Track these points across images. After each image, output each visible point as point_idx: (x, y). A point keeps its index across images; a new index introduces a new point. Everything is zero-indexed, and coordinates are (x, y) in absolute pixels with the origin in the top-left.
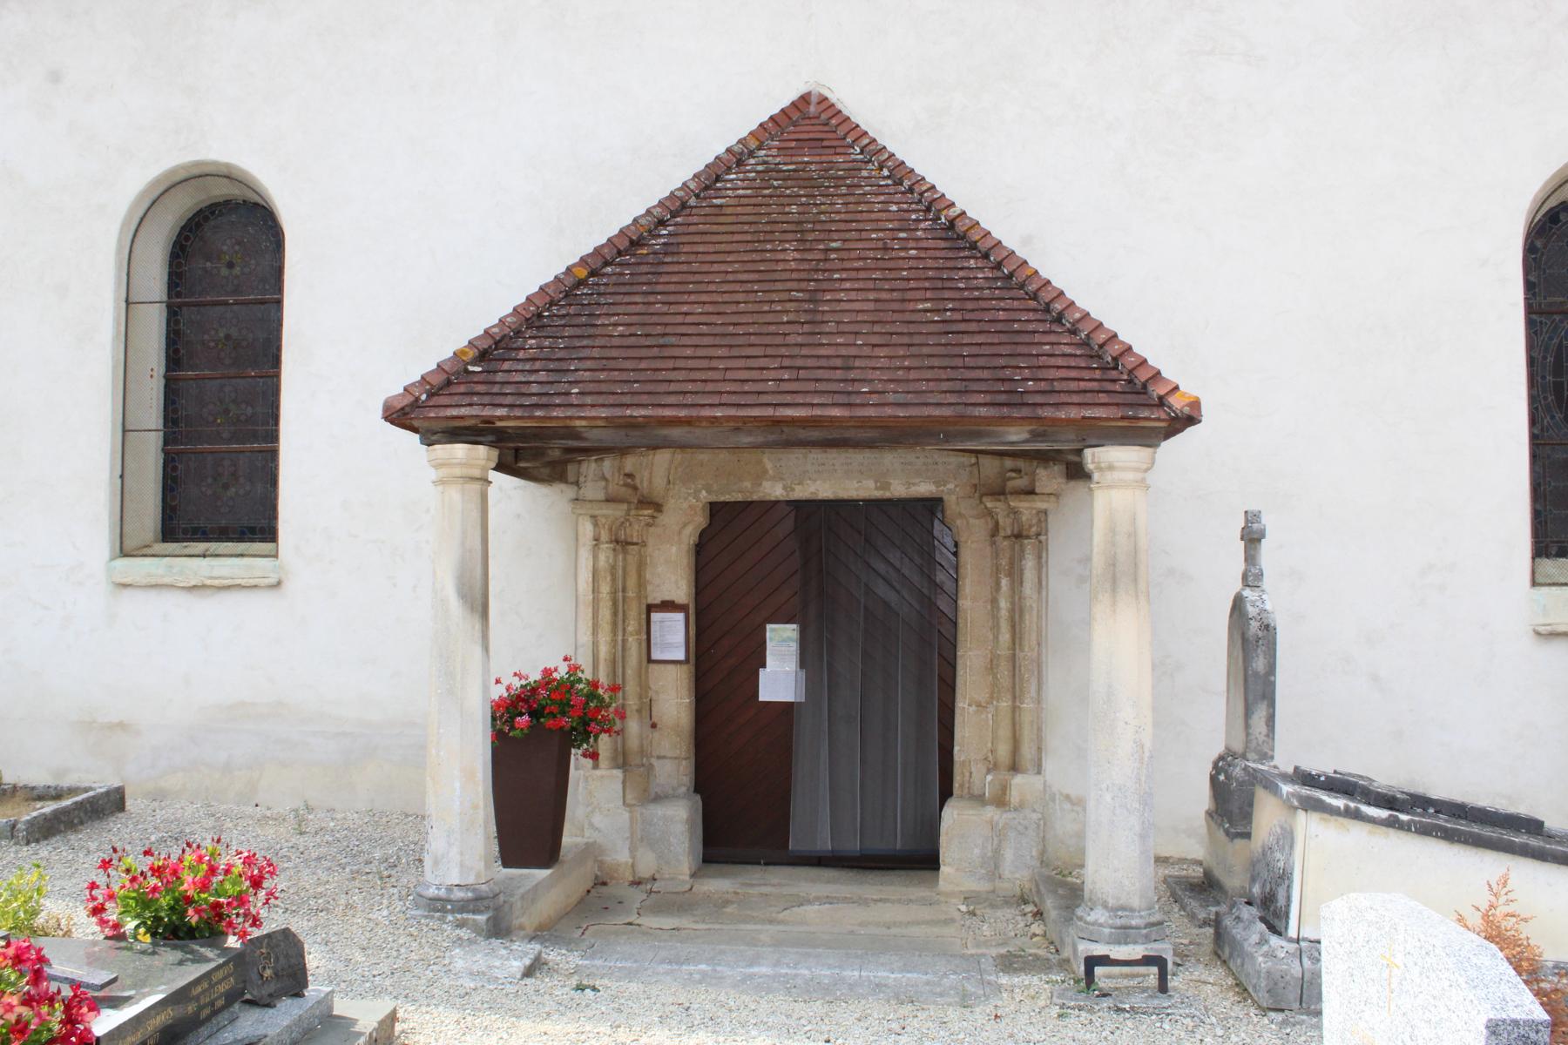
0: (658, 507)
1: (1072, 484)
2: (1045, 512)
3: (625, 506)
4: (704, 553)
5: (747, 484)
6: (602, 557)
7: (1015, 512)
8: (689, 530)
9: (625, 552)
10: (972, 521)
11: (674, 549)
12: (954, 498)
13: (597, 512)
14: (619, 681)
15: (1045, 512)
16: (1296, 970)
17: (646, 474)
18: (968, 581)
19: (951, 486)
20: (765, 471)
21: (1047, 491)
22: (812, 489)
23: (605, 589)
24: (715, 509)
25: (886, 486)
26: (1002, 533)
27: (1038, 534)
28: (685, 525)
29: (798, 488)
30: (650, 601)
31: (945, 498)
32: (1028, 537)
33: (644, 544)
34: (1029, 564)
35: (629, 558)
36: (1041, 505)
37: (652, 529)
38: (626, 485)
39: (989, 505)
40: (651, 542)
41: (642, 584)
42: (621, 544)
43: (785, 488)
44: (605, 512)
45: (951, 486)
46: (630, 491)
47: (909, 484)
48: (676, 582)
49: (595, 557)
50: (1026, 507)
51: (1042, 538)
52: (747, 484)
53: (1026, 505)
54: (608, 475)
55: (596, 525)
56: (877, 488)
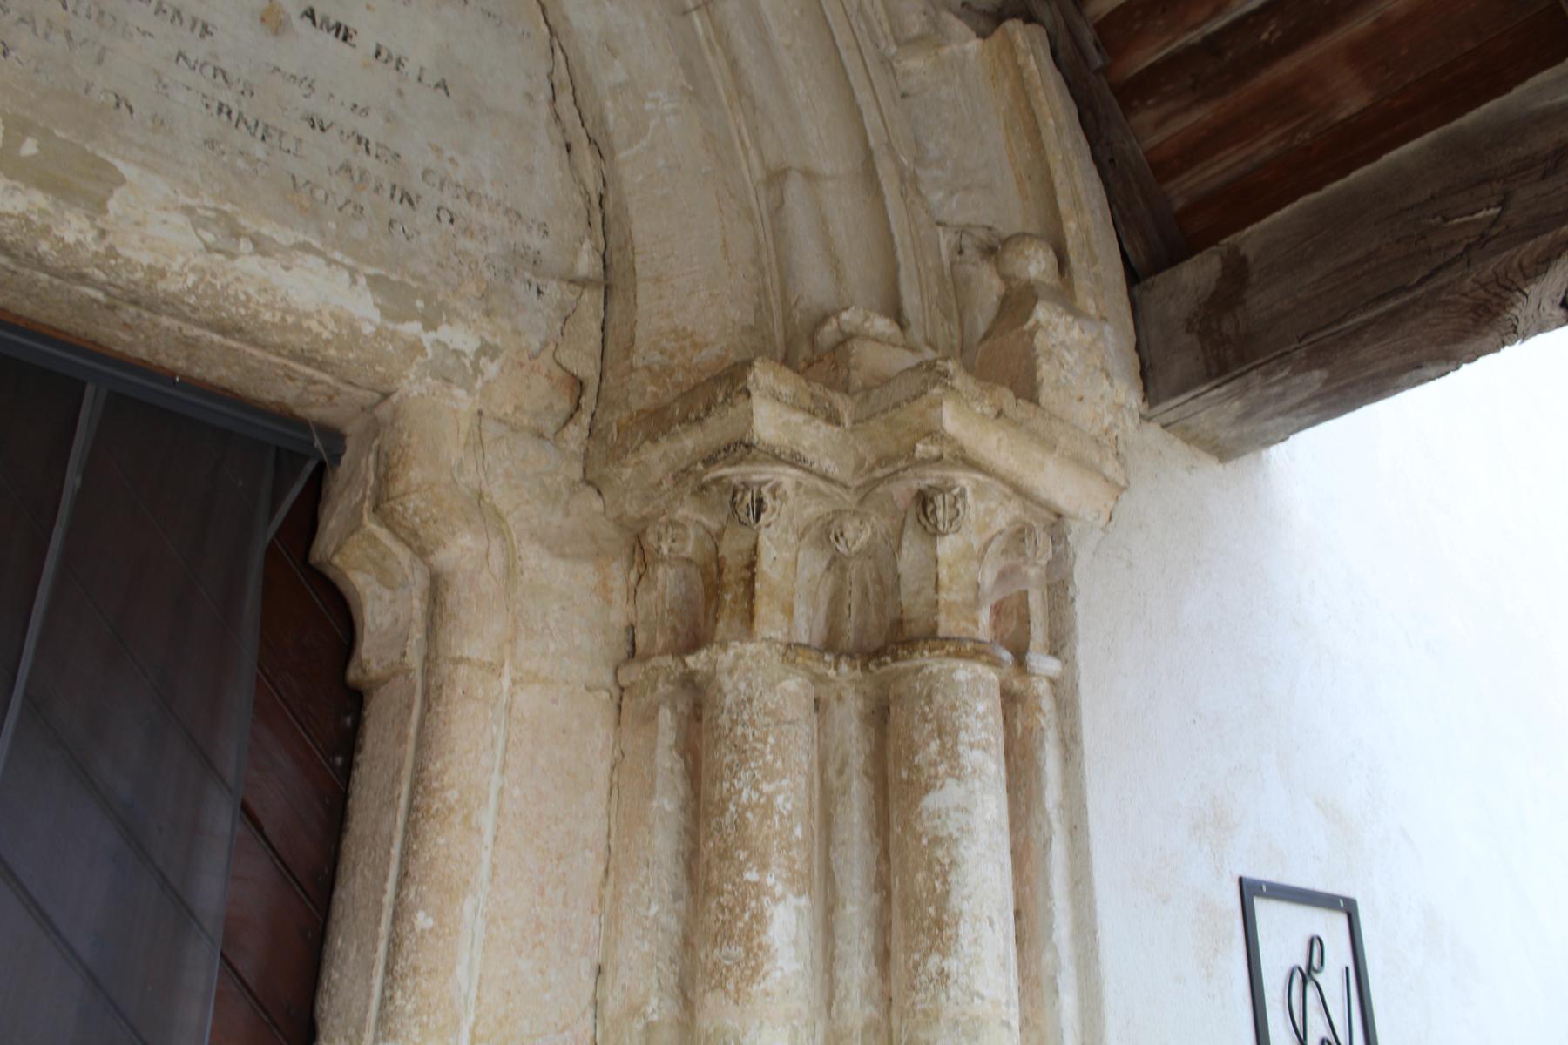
10: (533, 557)
12: (463, 401)
18: (471, 911)
19: (461, 337)
26: (770, 622)
31: (413, 385)
34: (971, 806)
45: (461, 337)
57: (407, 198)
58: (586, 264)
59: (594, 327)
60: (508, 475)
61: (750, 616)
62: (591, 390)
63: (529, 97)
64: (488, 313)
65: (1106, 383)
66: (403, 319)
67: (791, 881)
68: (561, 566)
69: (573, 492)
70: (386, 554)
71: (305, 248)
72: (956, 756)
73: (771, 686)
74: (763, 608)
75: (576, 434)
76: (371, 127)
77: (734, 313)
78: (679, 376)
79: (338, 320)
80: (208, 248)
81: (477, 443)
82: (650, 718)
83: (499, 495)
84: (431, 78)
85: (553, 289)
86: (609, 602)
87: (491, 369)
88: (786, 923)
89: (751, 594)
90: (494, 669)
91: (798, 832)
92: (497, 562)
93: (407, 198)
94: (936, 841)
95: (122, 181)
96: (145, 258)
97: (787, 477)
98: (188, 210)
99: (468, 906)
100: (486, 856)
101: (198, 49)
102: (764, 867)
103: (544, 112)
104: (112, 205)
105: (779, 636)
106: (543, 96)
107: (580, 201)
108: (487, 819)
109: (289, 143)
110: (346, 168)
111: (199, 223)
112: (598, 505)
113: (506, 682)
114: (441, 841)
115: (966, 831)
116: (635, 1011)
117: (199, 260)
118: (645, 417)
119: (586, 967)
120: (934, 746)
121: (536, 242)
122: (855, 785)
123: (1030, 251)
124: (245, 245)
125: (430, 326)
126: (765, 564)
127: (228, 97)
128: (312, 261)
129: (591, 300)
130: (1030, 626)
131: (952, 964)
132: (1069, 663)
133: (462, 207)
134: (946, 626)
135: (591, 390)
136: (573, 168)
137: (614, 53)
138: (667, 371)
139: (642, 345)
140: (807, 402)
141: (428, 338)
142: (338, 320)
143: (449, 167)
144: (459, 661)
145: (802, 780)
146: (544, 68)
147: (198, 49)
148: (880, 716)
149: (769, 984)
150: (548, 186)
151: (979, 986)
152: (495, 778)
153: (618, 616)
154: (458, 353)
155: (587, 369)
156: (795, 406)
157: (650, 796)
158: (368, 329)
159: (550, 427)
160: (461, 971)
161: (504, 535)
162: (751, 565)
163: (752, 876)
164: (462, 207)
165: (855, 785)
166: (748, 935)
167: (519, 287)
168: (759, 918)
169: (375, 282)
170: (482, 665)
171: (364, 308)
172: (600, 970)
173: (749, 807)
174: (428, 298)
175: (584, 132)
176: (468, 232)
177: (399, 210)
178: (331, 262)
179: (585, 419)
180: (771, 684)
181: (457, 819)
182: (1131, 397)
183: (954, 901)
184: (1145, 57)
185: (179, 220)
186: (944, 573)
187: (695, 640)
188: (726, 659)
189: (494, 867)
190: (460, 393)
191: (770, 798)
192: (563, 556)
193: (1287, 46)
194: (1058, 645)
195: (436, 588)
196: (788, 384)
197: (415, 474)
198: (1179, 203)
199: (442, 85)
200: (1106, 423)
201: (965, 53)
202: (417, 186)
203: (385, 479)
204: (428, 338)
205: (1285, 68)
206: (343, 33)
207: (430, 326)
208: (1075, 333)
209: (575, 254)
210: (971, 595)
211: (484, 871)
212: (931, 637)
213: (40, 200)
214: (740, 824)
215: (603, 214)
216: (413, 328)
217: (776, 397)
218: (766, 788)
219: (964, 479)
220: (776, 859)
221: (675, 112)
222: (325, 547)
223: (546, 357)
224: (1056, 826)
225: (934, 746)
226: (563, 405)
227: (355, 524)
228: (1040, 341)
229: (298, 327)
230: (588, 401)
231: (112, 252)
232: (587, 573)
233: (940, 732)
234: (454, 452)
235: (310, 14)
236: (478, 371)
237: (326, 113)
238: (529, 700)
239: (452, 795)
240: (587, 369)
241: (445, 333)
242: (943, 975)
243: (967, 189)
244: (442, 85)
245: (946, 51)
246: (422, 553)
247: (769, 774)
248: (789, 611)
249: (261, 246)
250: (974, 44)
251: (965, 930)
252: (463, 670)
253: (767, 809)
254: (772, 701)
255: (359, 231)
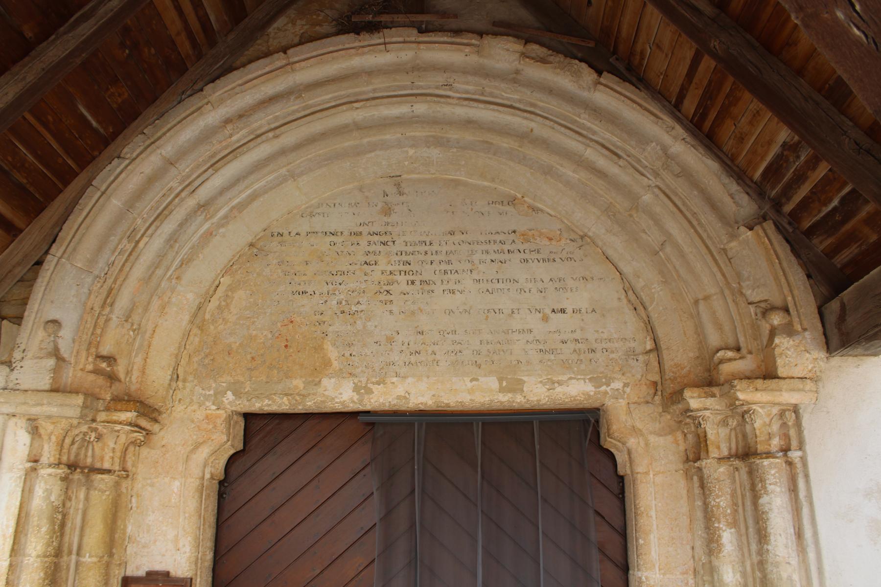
0: (148, 411)
1: (836, 360)
2: (796, 410)
3: (79, 400)
4: (229, 492)
5: (298, 383)
6: (39, 491)
7: (744, 415)
8: (204, 452)
9: (89, 486)
10: (652, 439)
11: (177, 483)
12: (623, 402)
13: (35, 410)
14: (737, 473)
15: (796, 410)
16: (75, 300)
17: (138, 360)
18: (653, 538)
19: (617, 385)
20: (327, 363)
21: (798, 372)
22: (400, 391)
23: (36, 546)
24: (255, 424)
25: (516, 386)
26: (714, 453)
27: (786, 450)
28: (197, 446)
29: (377, 389)
30: (131, 571)
31: (609, 402)
32: (769, 455)
33: (126, 473)
34: (776, 502)
35: (94, 494)
36: (789, 398)
37: (145, 451)
38: (96, 371)
39: (694, 404)
40: (141, 471)
41: (113, 540)
42: (76, 469)
43: (356, 389)
44: (54, 410)
45: (617, 385)
46: (101, 381)
47: (552, 383)
48: (176, 539)
49: (27, 492)
50: (762, 401)
51: (795, 455)
52: (298, 383)
53: (759, 396)
54: (65, 352)
55: (35, 431)
56: (502, 390)
57: (593, 351)
58: (649, 345)
59: (656, 364)
60: (640, 418)
61: (707, 452)
62: (659, 383)
63: (619, 299)
64: (623, 374)
65: (807, 355)
66: (600, 387)
67: (728, 525)
68: (661, 439)
69: (661, 416)
70: (615, 445)
71: (571, 378)
72: (766, 488)
73: (715, 471)
74: (710, 449)
75: (657, 398)
76: (577, 335)
77: (691, 355)
78: (679, 380)
79: (583, 394)
80: (549, 390)
81: (629, 412)
82: (692, 479)
83: (639, 425)
84: (590, 311)
85: (641, 358)
86: (678, 445)
87: (628, 390)
88: (727, 537)
89: (707, 445)
90: (647, 473)
91: (729, 511)
92: (642, 444)
93: (593, 351)
94: (763, 513)
95: (525, 382)
96: (535, 399)
97: (707, 413)
98: (541, 382)
99: (652, 536)
100: (654, 523)
101: (530, 337)
102: (719, 523)
103: (625, 301)
104: (525, 389)
105: (716, 456)
106: (623, 297)
107: (642, 324)
108: (653, 513)
109: (559, 351)
110: (575, 351)
111: (544, 384)
112: (669, 417)
113: (651, 476)
114: (642, 521)
115: (771, 510)
116: (700, 560)
117: (547, 394)
118: (668, 394)
119: (688, 547)
120: (760, 485)
121: (632, 345)
122: (748, 494)
123: (773, 317)
124: (556, 385)
125: (608, 385)
126: (709, 436)
127: (541, 347)
128: (573, 381)
129: (653, 357)
130: (791, 442)
131: (770, 547)
132: (804, 452)
133: (609, 345)
134: (761, 448)
135: (659, 383)
136: (638, 315)
137: (639, 277)
138: (675, 378)
139: (667, 372)
140: (703, 395)
141: (608, 389)
142: (583, 394)
143: (602, 335)
144: (637, 473)
145: (728, 497)
146: (621, 286)
147: (530, 337)
148: (750, 473)
149: (724, 554)
150: (632, 325)
151: (777, 553)
152: (654, 502)
153: (682, 448)
154: (617, 390)
155: (657, 378)
156: (699, 397)
157: (695, 501)
158: (592, 393)
159: (649, 399)
160: (653, 553)
161: (642, 435)
162: (705, 436)
163: (716, 525)
164: (609, 345)
165: (748, 494)
166: (717, 541)
167: (631, 362)
168: (719, 536)
169: (590, 380)
170: (643, 473)
171: (589, 388)
172: (693, 548)
173: (714, 506)
174: (605, 377)
175: (639, 305)
176: (612, 352)
177: (591, 355)
178: (578, 379)
179: (659, 393)
180: (717, 471)
181: (644, 515)
182: (823, 355)
183: (769, 530)
184: (807, 224)
185: (540, 385)
186: (758, 432)
187: (698, 459)
188: (704, 463)
189: (657, 526)
190: (621, 401)
191: (719, 503)
192: (661, 436)
193: (843, 222)
194: (801, 447)
195: (629, 453)
196: (696, 392)
197: (614, 427)
198: (839, 266)
199: (594, 310)
200: (810, 368)
201: (747, 237)
202: (595, 346)
203: (608, 429)
204: (608, 389)
205: (848, 226)
206: (563, 311)
207: (608, 385)
208: (791, 342)
209: (645, 343)
210: (767, 437)
211: (655, 527)
212: (756, 454)
213: (510, 395)
214: (712, 511)
215: (650, 328)
216: (604, 388)
217: (692, 397)
218: (717, 500)
219: (754, 407)
220: (723, 520)
221: (661, 290)
222: (602, 443)
223: (644, 379)
224: (804, 503)
225: (760, 485)
226: (652, 391)
227: (606, 440)
228: (777, 351)
229: (575, 400)
230: (659, 387)
231: (528, 400)
232: (670, 438)
233: (761, 481)
234: (623, 417)
235: (553, 311)
236: (624, 392)
237: (564, 337)
238: (659, 479)
239: (642, 509)
240: (657, 378)
241: (613, 385)
242: (768, 550)
243: (758, 287)
244: (594, 310)
245: (741, 238)
246: (624, 444)
247: (718, 496)
248: (718, 448)
249: (560, 383)
250: (749, 233)
251: (772, 538)
252: (639, 476)
253: (718, 507)
254: (716, 475)
255: (583, 367)
